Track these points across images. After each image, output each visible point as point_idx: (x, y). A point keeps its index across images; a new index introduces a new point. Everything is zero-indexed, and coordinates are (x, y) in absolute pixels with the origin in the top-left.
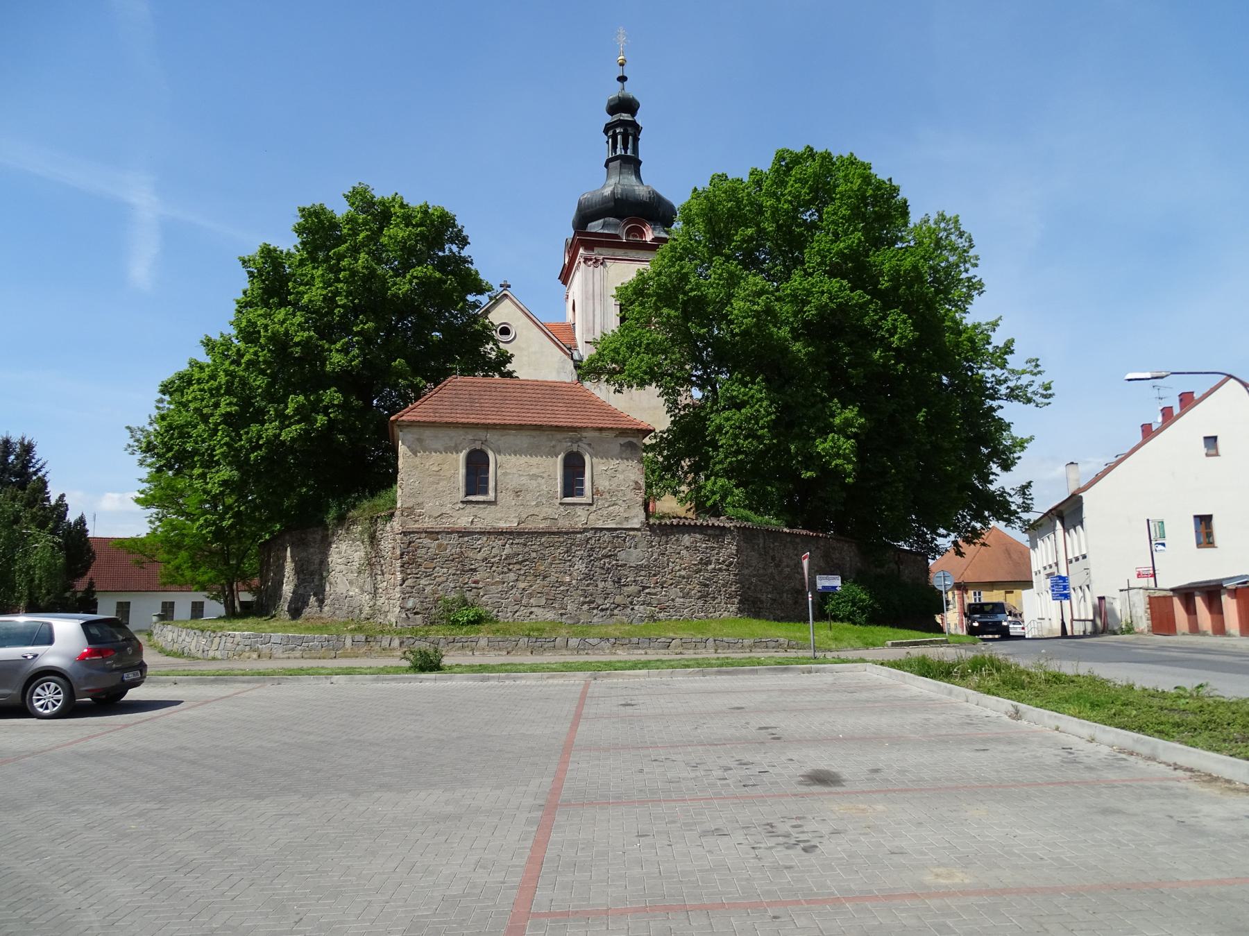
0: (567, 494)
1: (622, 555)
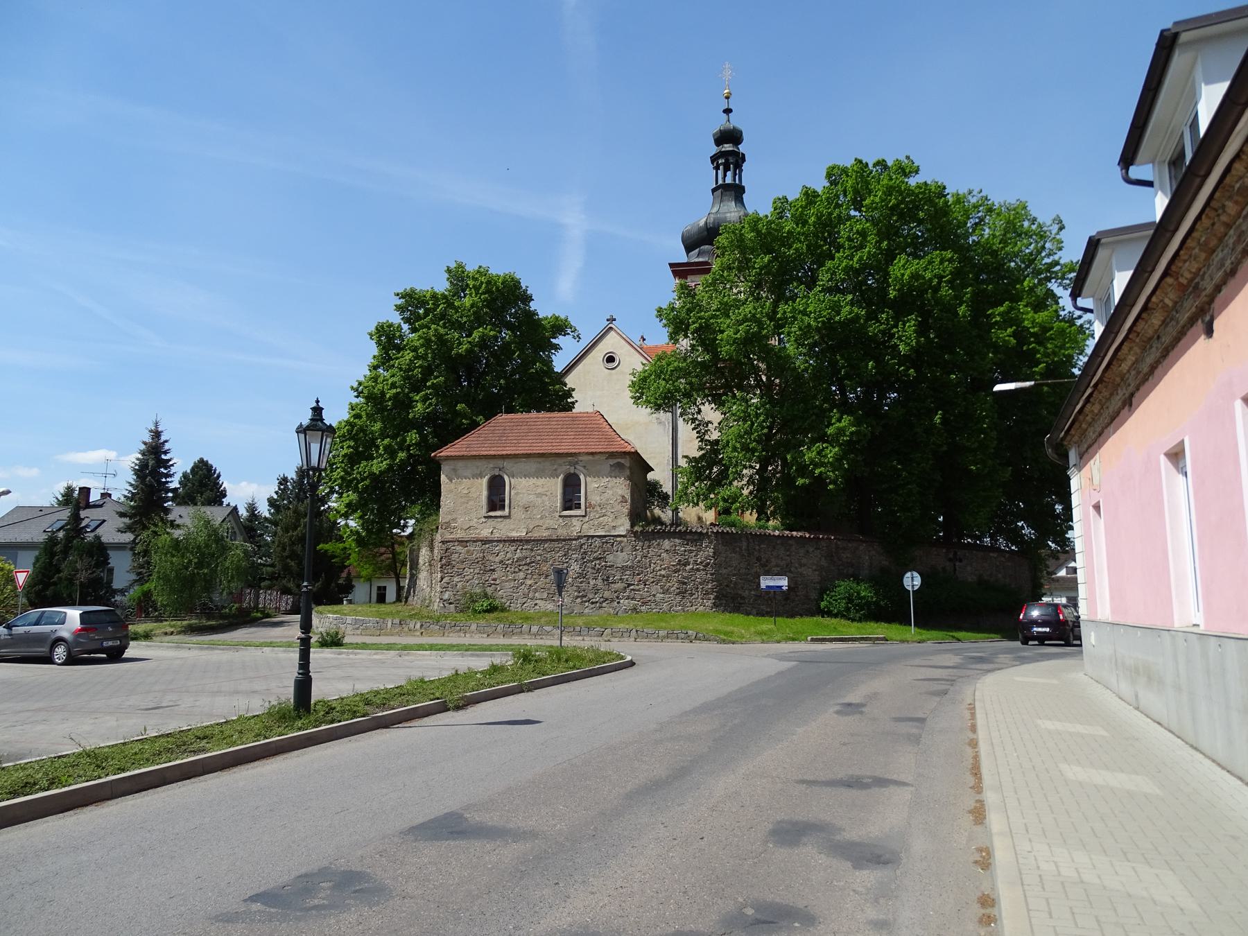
1: (610, 558)
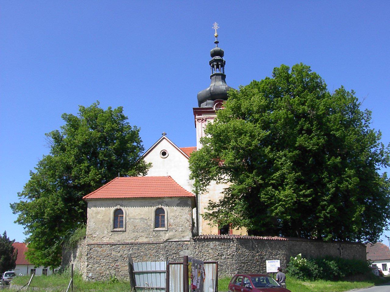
0: (157, 225)
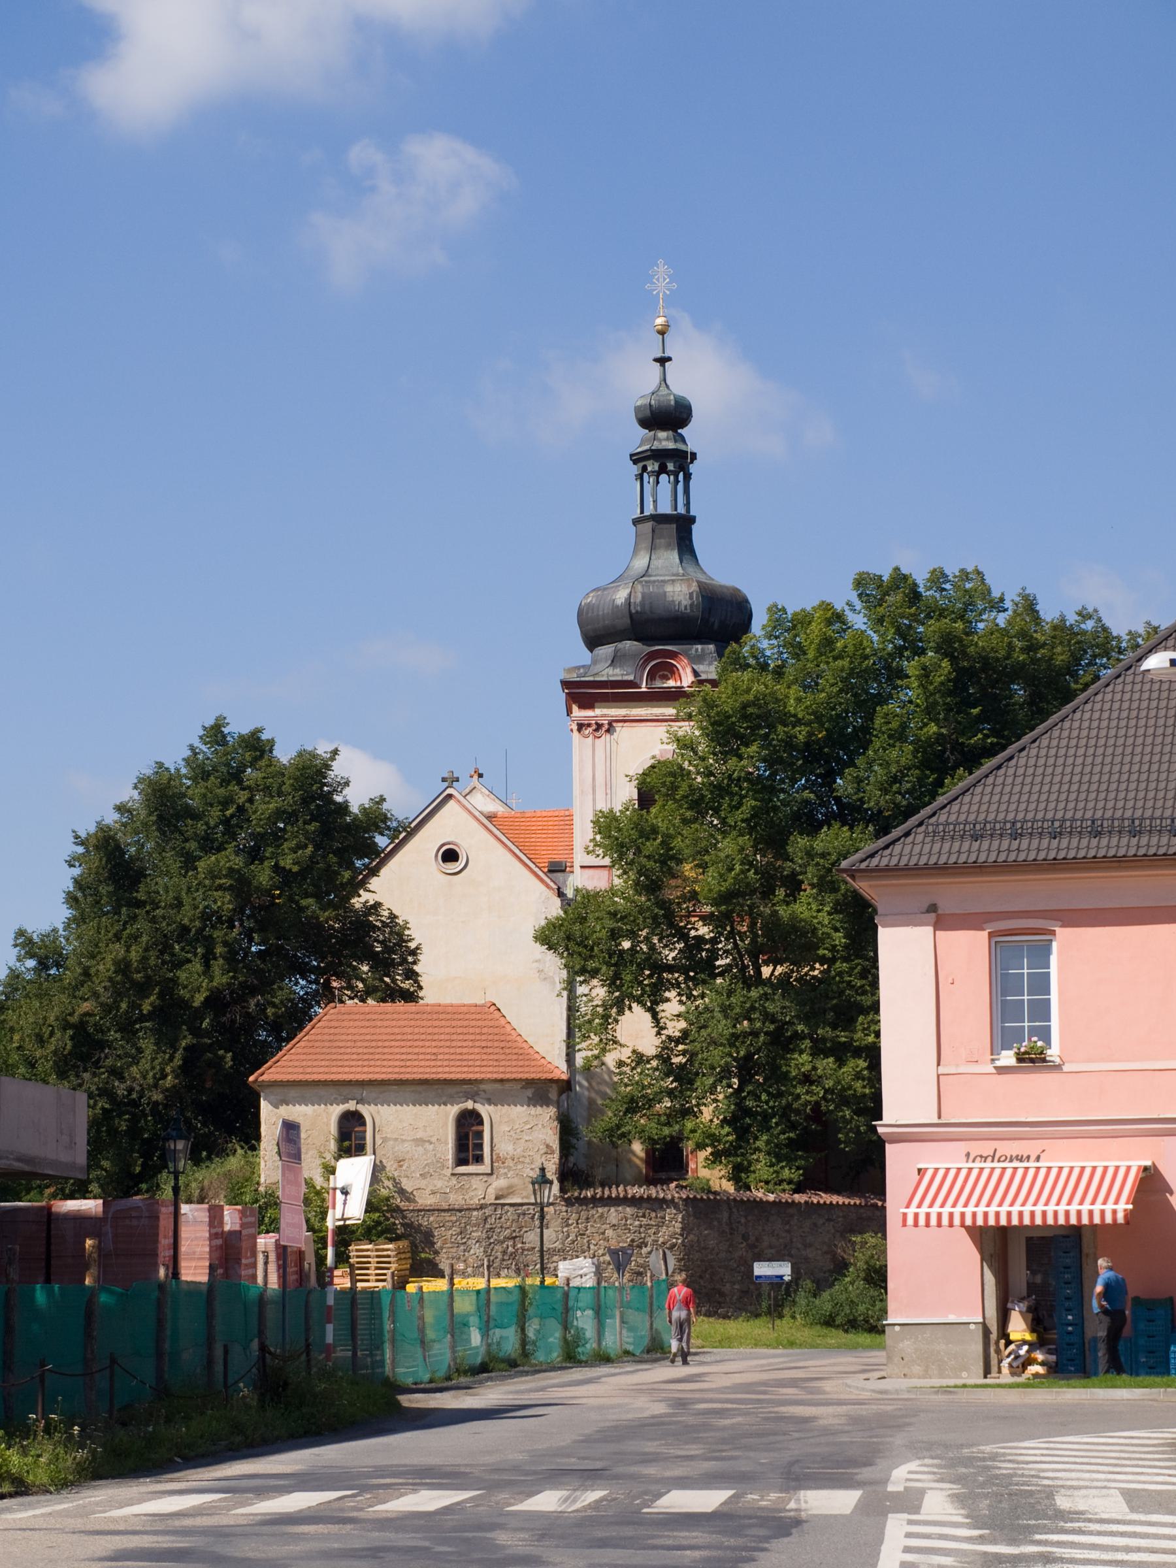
0: (461, 1161)
